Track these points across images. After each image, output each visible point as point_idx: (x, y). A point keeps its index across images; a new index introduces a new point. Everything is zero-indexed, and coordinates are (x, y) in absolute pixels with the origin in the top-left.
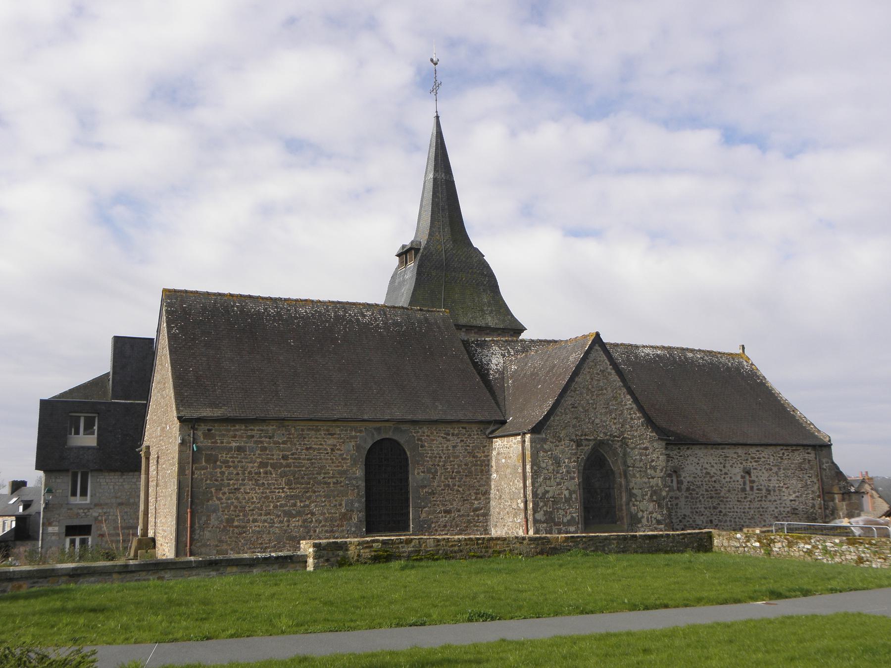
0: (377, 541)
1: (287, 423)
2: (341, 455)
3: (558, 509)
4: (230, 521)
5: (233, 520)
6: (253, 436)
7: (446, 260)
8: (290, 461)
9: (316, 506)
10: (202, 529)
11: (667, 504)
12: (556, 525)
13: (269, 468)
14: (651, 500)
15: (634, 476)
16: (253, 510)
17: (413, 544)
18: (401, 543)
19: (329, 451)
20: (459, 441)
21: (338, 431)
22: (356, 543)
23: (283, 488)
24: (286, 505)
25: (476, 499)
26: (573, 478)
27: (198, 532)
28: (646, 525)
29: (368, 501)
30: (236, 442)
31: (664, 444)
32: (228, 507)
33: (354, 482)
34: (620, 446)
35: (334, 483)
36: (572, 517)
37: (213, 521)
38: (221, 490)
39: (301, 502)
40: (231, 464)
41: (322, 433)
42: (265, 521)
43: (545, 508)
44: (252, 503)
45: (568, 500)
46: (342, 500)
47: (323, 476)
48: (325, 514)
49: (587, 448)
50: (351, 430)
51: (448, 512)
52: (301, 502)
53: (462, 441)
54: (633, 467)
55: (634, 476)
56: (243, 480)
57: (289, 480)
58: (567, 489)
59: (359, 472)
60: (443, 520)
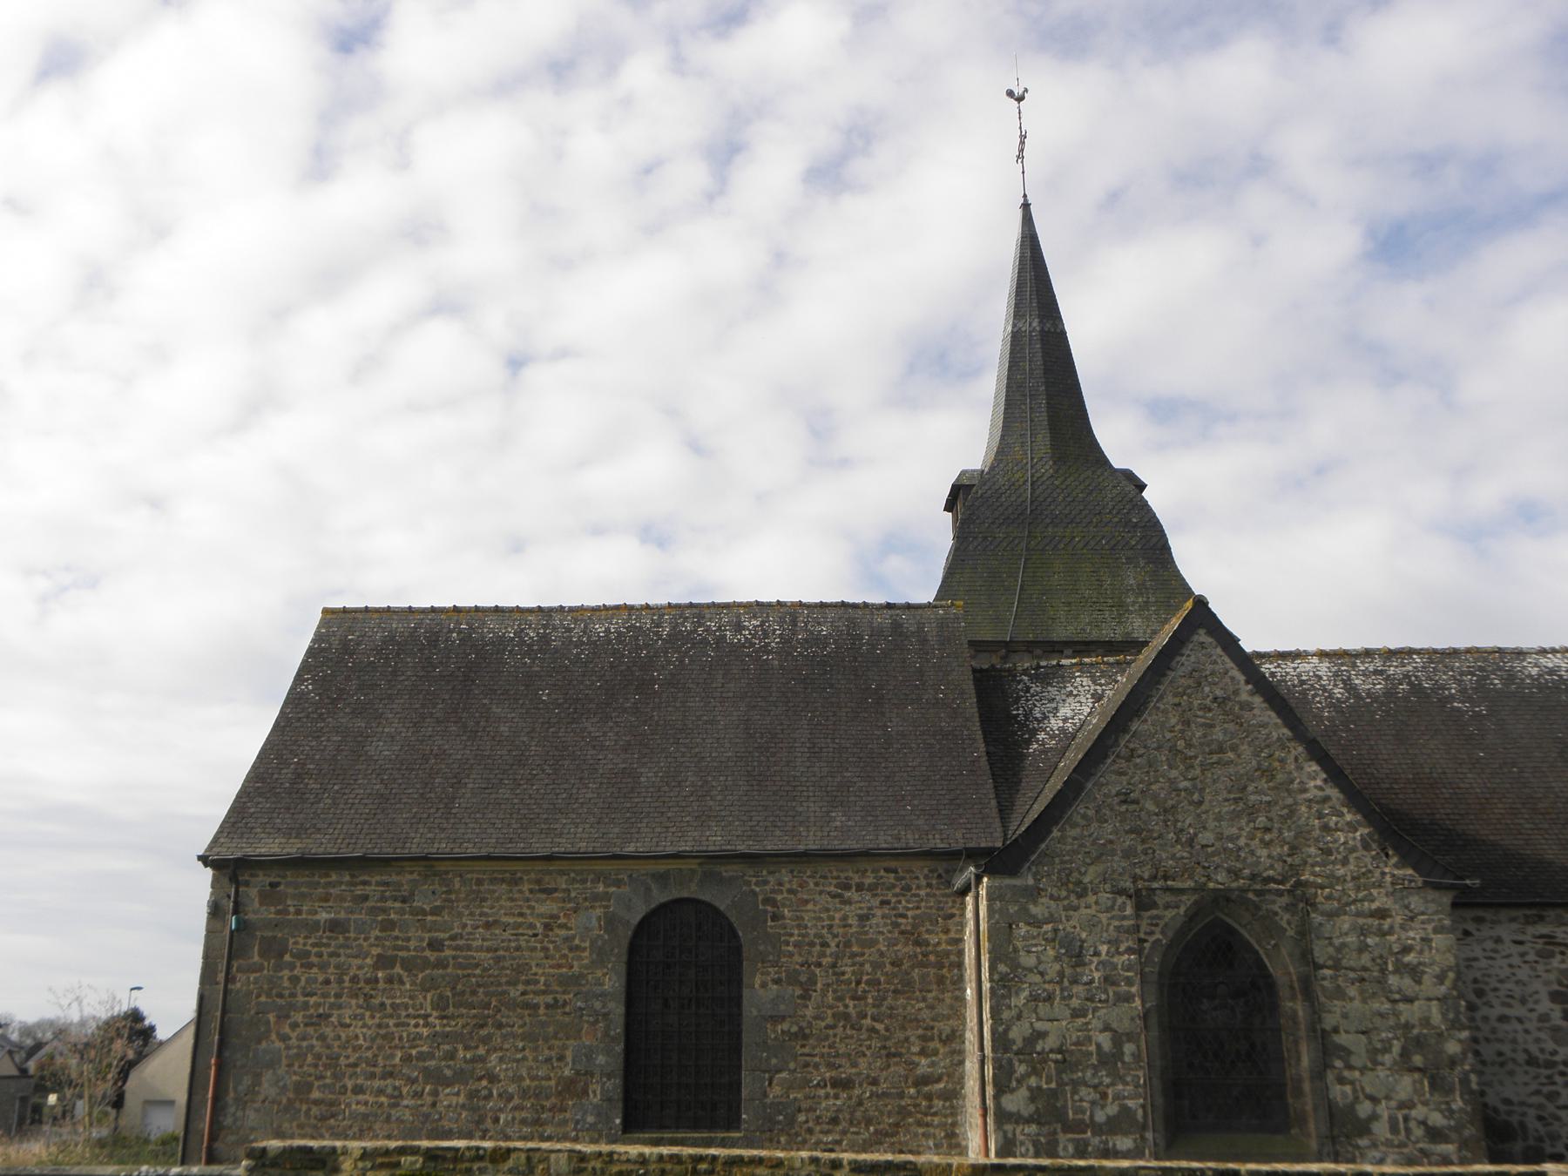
0: (415, 1151)
1: (441, 867)
2: (567, 939)
3: (1076, 1084)
4: (303, 1088)
5: (310, 1087)
6: (366, 898)
7: (1052, 502)
8: (448, 953)
9: (501, 1060)
10: (242, 1103)
11: (1465, 1081)
12: (1067, 1128)
13: (398, 970)
14: (1404, 1064)
15: (1340, 993)
16: (355, 1065)
17: (510, 1163)
18: (480, 1158)
19: (540, 929)
20: (876, 902)
21: (562, 883)
22: (357, 1154)
23: (426, 1016)
24: (431, 1056)
25: (923, 1052)
26: (1128, 998)
27: (232, 1110)
28: (1388, 1143)
29: (628, 1051)
30: (328, 910)
31: (1447, 899)
32: (301, 1056)
33: (598, 1005)
34: (1286, 908)
35: (548, 1006)
36: (1124, 1108)
37: (267, 1088)
38: (288, 1017)
39: (466, 1048)
40: (314, 959)
41: (526, 888)
42: (381, 1092)
43: (1033, 1081)
44: (356, 1049)
45: (1109, 1060)
46: (565, 1047)
47: (521, 987)
48: (521, 1078)
49: (1169, 914)
50: (596, 880)
51: (843, 1084)
52: (466, 1048)
53: (883, 903)
54: (1336, 966)
55: (1340, 993)
56: (338, 996)
57: (441, 997)
58: (1107, 1028)
59: (611, 981)
60: (830, 1104)
